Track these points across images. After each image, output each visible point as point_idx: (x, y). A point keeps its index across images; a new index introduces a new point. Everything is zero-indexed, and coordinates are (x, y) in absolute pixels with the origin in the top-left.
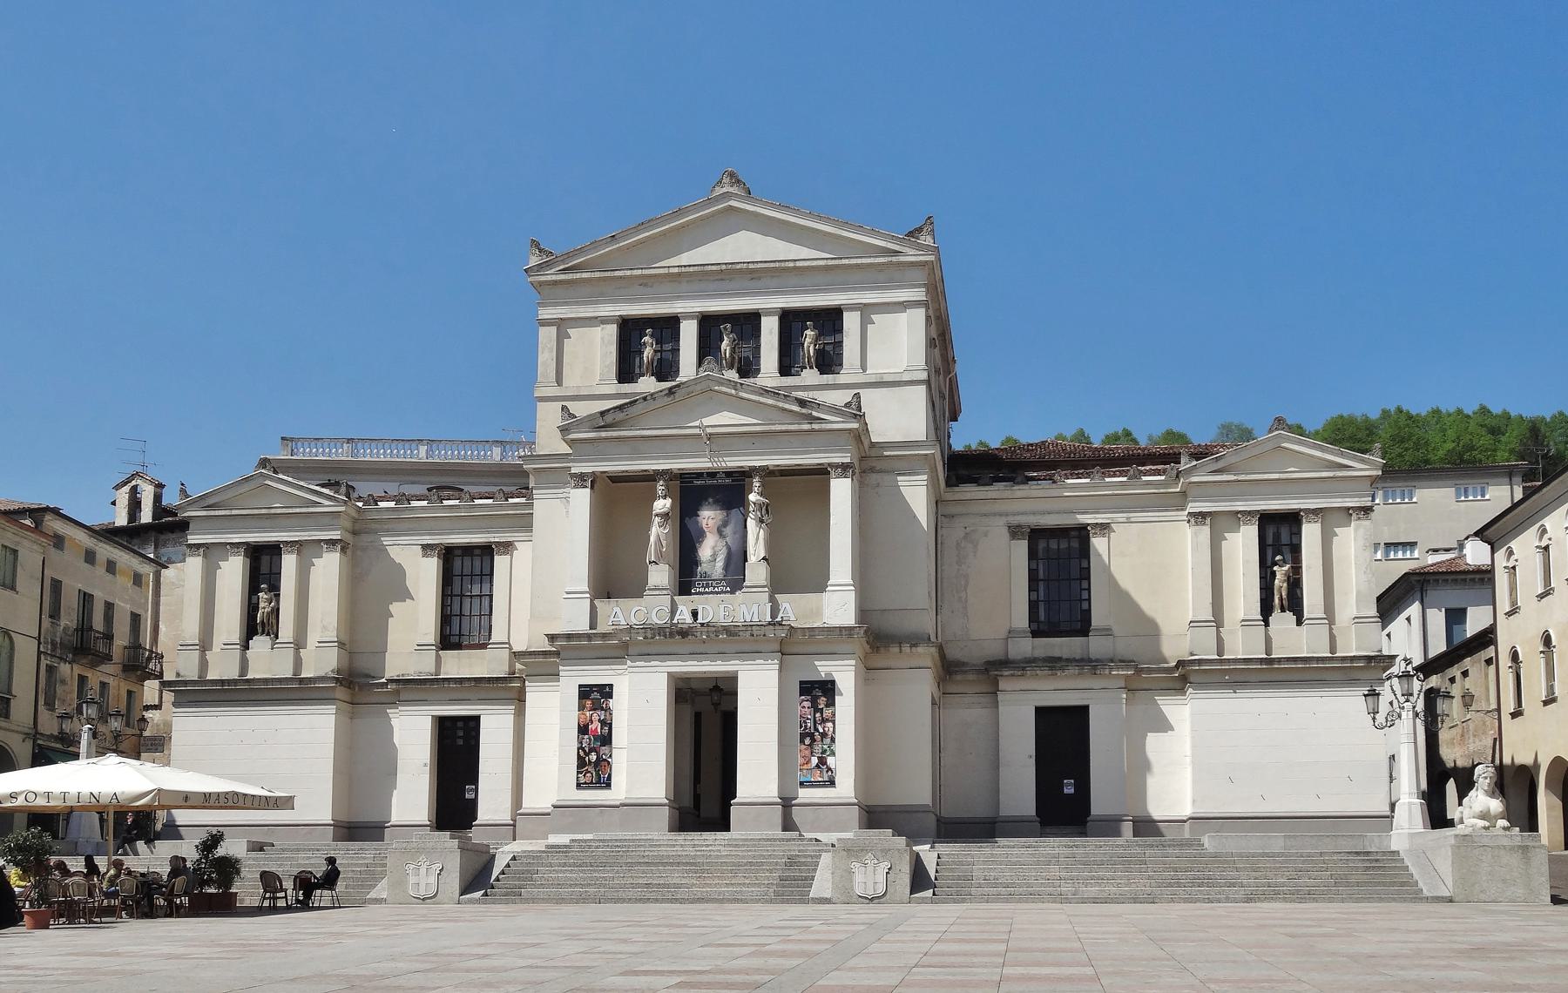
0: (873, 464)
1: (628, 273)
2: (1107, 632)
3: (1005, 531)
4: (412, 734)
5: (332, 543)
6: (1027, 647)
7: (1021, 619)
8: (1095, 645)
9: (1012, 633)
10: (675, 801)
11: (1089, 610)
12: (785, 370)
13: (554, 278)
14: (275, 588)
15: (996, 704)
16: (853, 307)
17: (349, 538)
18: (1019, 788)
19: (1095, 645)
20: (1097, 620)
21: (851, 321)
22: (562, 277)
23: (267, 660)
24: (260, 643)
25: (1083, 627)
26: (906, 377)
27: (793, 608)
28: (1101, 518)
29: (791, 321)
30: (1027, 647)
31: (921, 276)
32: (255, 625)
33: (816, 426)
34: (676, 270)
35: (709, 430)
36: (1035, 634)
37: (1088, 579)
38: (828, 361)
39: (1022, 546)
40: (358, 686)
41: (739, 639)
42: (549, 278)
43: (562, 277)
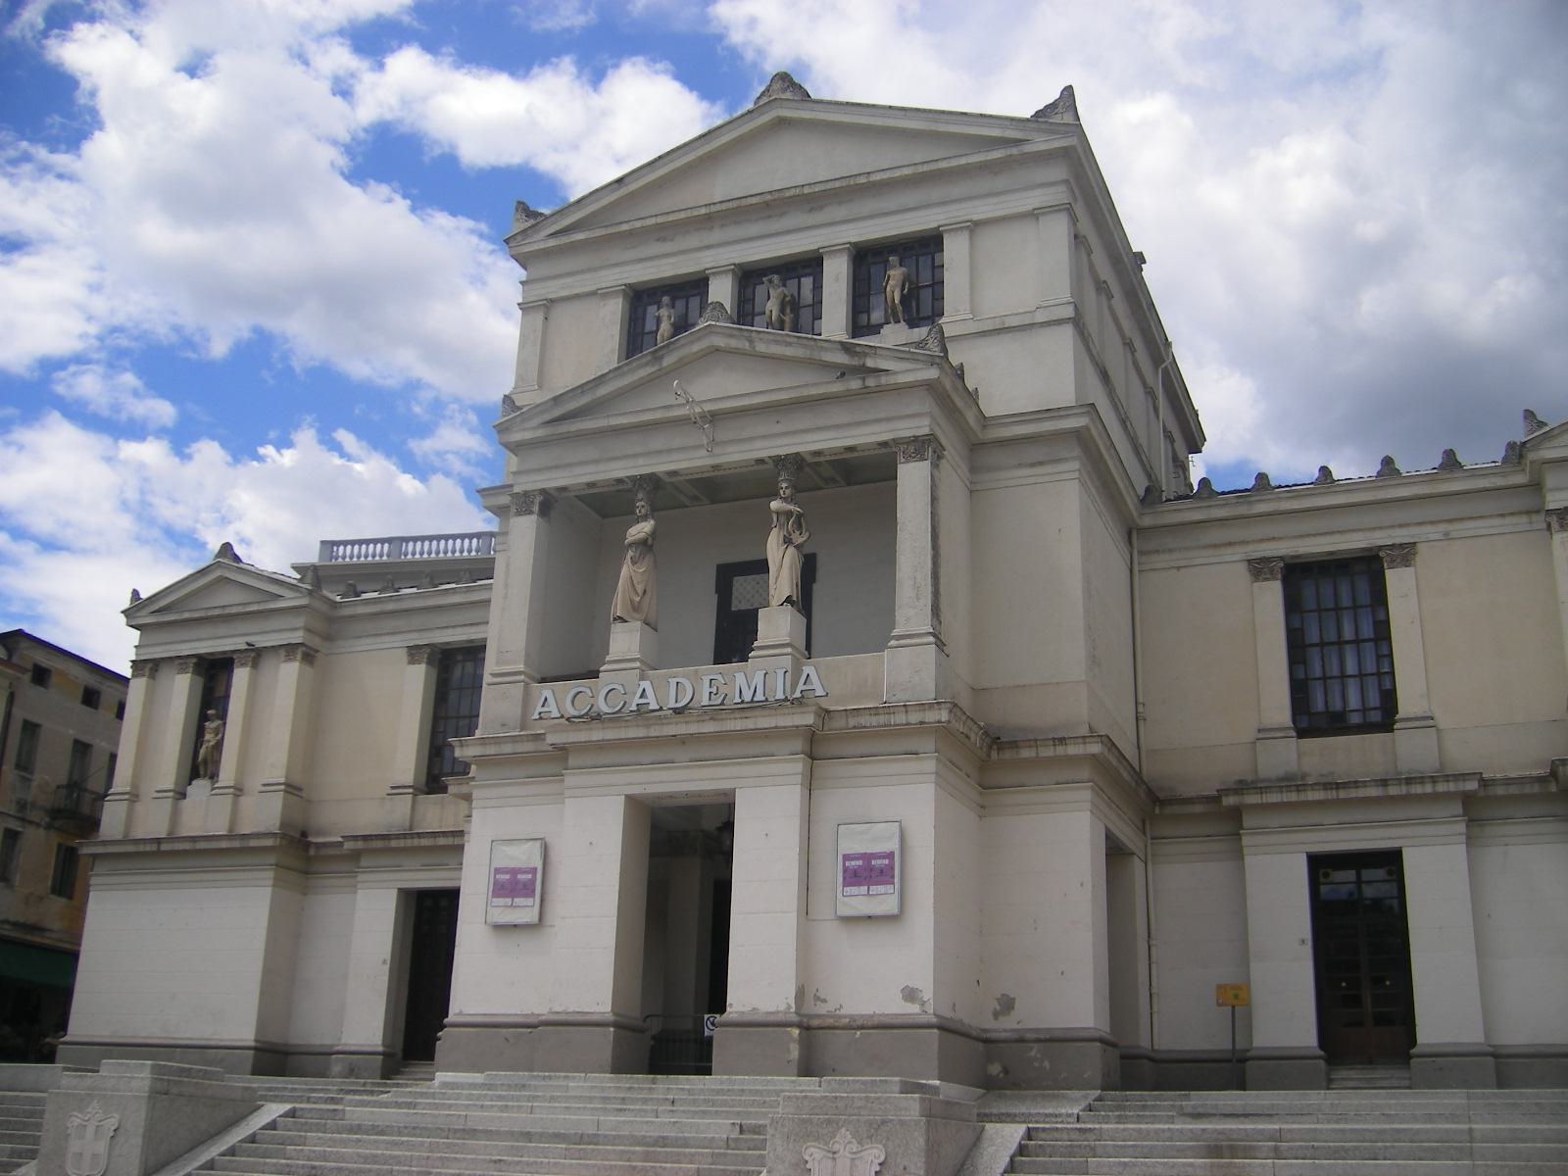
0: (981, 445)
1: (638, 224)
2: (1426, 721)
3: (1243, 568)
4: (367, 924)
5: (290, 649)
6: (1289, 755)
7: (1278, 708)
8: (1408, 748)
9: (1265, 733)
10: (622, 1026)
11: (1394, 690)
12: (860, 325)
13: (542, 246)
14: (223, 716)
15: (1239, 855)
16: (957, 228)
17: (315, 642)
18: (1288, 1008)
19: (1408, 748)
20: (1408, 702)
21: (955, 251)
22: (552, 243)
23: (205, 813)
24: (199, 788)
25: (1384, 716)
26: (1040, 318)
27: (833, 678)
28: (1400, 536)
29: (867, 258)
30: (1289, 755)
31: (1059, 172)
32: (200, 765)
33: (871, 382)
34: (703, 211)
35: (708, 407)
36: (1302, 733)
37: (1389, 638)
38: (922, 304)
39: (1271, 596)
40: (303, 854)
41: (736, 733)
42: (536, 247)
43: (552, 243)
